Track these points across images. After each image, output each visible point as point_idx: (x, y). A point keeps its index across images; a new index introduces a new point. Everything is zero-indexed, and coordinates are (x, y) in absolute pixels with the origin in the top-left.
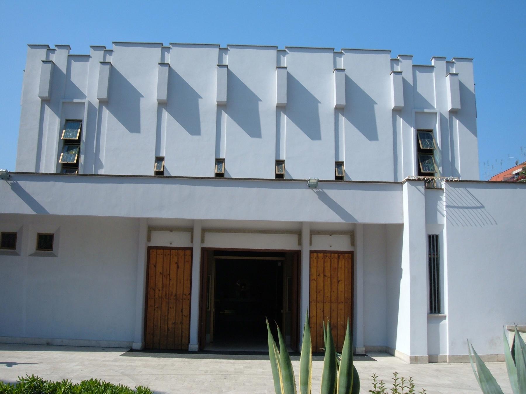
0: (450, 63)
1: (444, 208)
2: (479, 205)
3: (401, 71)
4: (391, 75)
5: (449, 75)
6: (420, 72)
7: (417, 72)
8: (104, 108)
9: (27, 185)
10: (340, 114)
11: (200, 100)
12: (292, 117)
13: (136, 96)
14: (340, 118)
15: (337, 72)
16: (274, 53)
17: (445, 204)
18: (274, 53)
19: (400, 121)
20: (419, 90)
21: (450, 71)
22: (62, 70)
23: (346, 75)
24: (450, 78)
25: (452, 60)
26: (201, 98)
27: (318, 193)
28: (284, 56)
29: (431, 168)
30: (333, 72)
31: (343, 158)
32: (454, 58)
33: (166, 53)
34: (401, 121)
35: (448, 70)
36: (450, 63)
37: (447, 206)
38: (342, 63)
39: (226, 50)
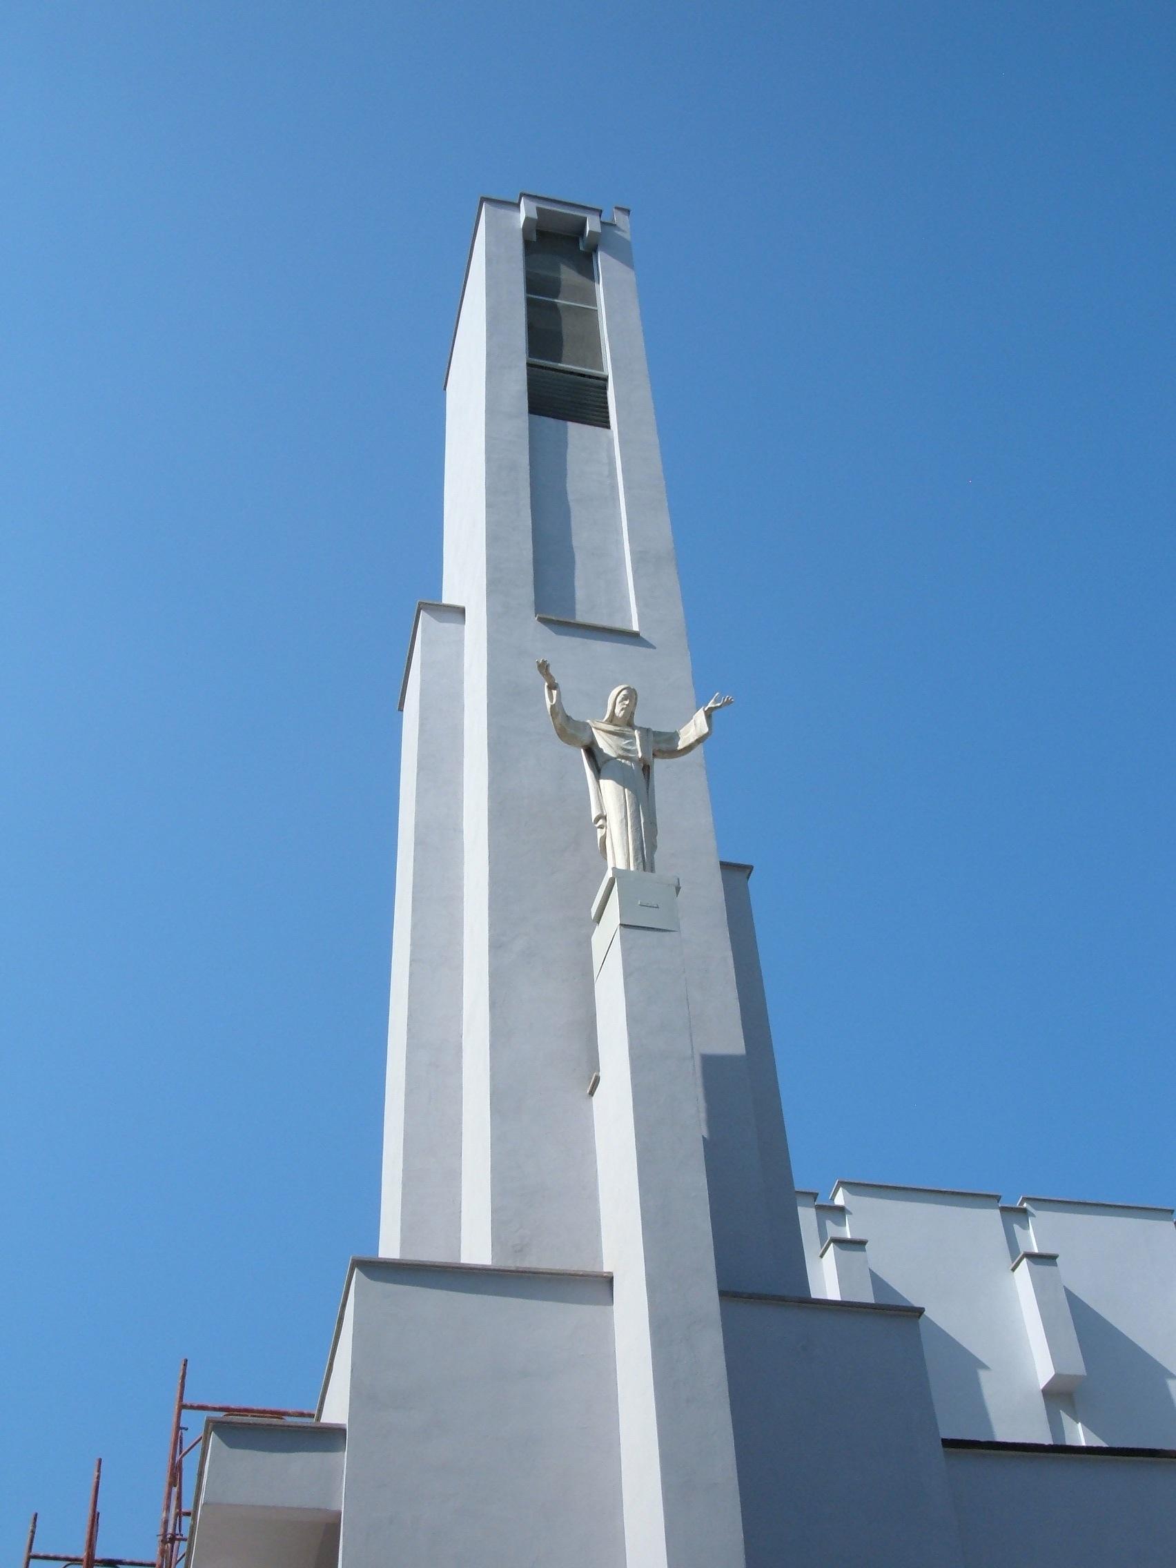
25: (1021, 1203)
32: (1026, 1199)
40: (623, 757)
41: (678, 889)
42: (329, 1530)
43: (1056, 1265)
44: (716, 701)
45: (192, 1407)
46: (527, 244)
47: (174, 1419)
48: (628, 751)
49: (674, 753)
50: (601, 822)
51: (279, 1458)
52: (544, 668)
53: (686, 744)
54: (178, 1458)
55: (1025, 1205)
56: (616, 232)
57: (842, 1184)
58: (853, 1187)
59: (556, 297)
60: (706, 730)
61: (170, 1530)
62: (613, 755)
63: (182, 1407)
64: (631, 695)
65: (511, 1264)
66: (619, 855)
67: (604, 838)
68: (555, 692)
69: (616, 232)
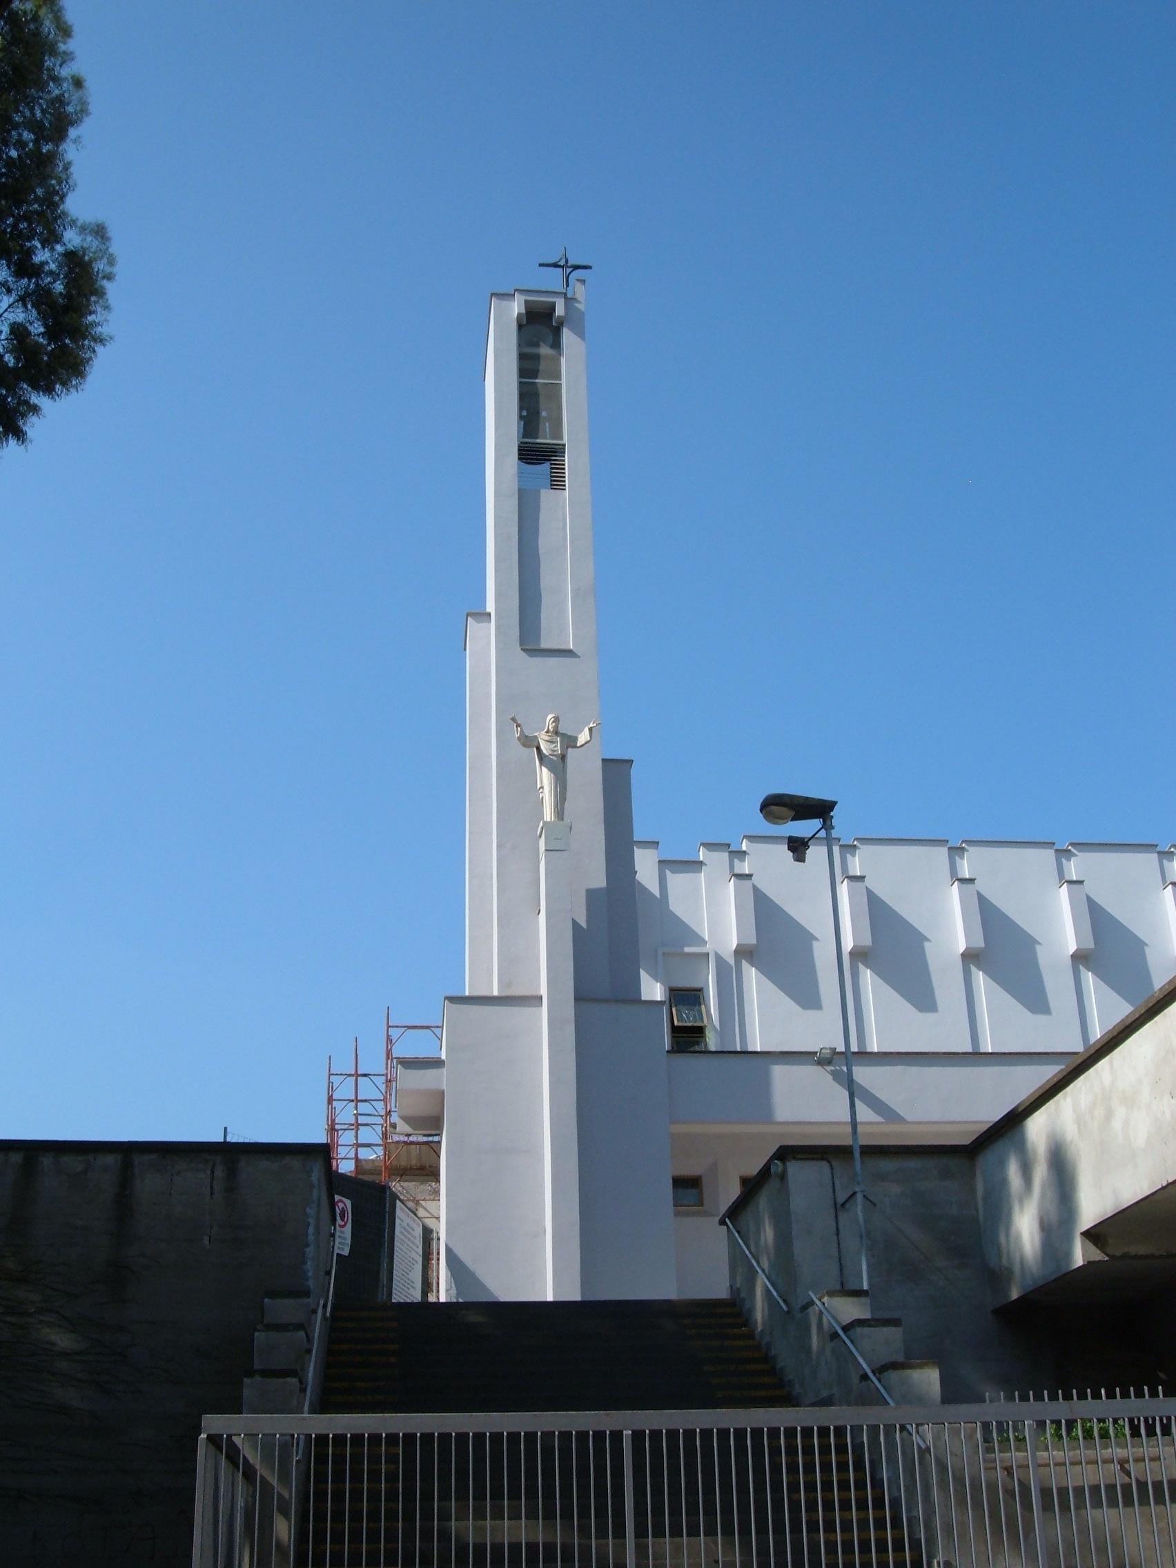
3: (863, 874)
4: (954, 886)
5: (956, 882)
6: (673, 872)
7: (668, 872)
8: (745, 964)
10: (743, 961)
11: (1146, 948)
12: (994, 974)
13: (806, 939)
14: (1082, 977)
15: (736, 880)
16: (1049, 854)
18: (1049, 854)
19: (1088, 976)
21: (957, 875)
22: (652, 890)
23: (754, 887)
24: (1068, 888)
25: (854, 842)
26: (928, 940)
28: (1069, 860)
30: (730, 881)
33: (957, 858)
38: (1073, 869)
39: (853, 848)
40: (551, 755)
41: (571, 829)
42: (443, 1093)
43: (864, 881)
44: (593, 723)
45: (392, 1027)
46: (520, 326)
47: (386, 1032)
48: (554, 751)
49: (575, 747)
50: (541, 790)
51: (422, 1072)
52: (513, 719)
53: (581, 744)
54: (389, 1047)
55: (855, 843)
56: (576, 305)
57: (745, 837)
58: (752, 838)
59: (536, 378)
60: (589, 739)
61: (389, 1077)
62: (548, 754)
63: (389, 1027)
64: (556, 720)
65: (503, 994)
66: (548, 814)
67: (543, 798)
68: (519, 729)
69: (576, 305)
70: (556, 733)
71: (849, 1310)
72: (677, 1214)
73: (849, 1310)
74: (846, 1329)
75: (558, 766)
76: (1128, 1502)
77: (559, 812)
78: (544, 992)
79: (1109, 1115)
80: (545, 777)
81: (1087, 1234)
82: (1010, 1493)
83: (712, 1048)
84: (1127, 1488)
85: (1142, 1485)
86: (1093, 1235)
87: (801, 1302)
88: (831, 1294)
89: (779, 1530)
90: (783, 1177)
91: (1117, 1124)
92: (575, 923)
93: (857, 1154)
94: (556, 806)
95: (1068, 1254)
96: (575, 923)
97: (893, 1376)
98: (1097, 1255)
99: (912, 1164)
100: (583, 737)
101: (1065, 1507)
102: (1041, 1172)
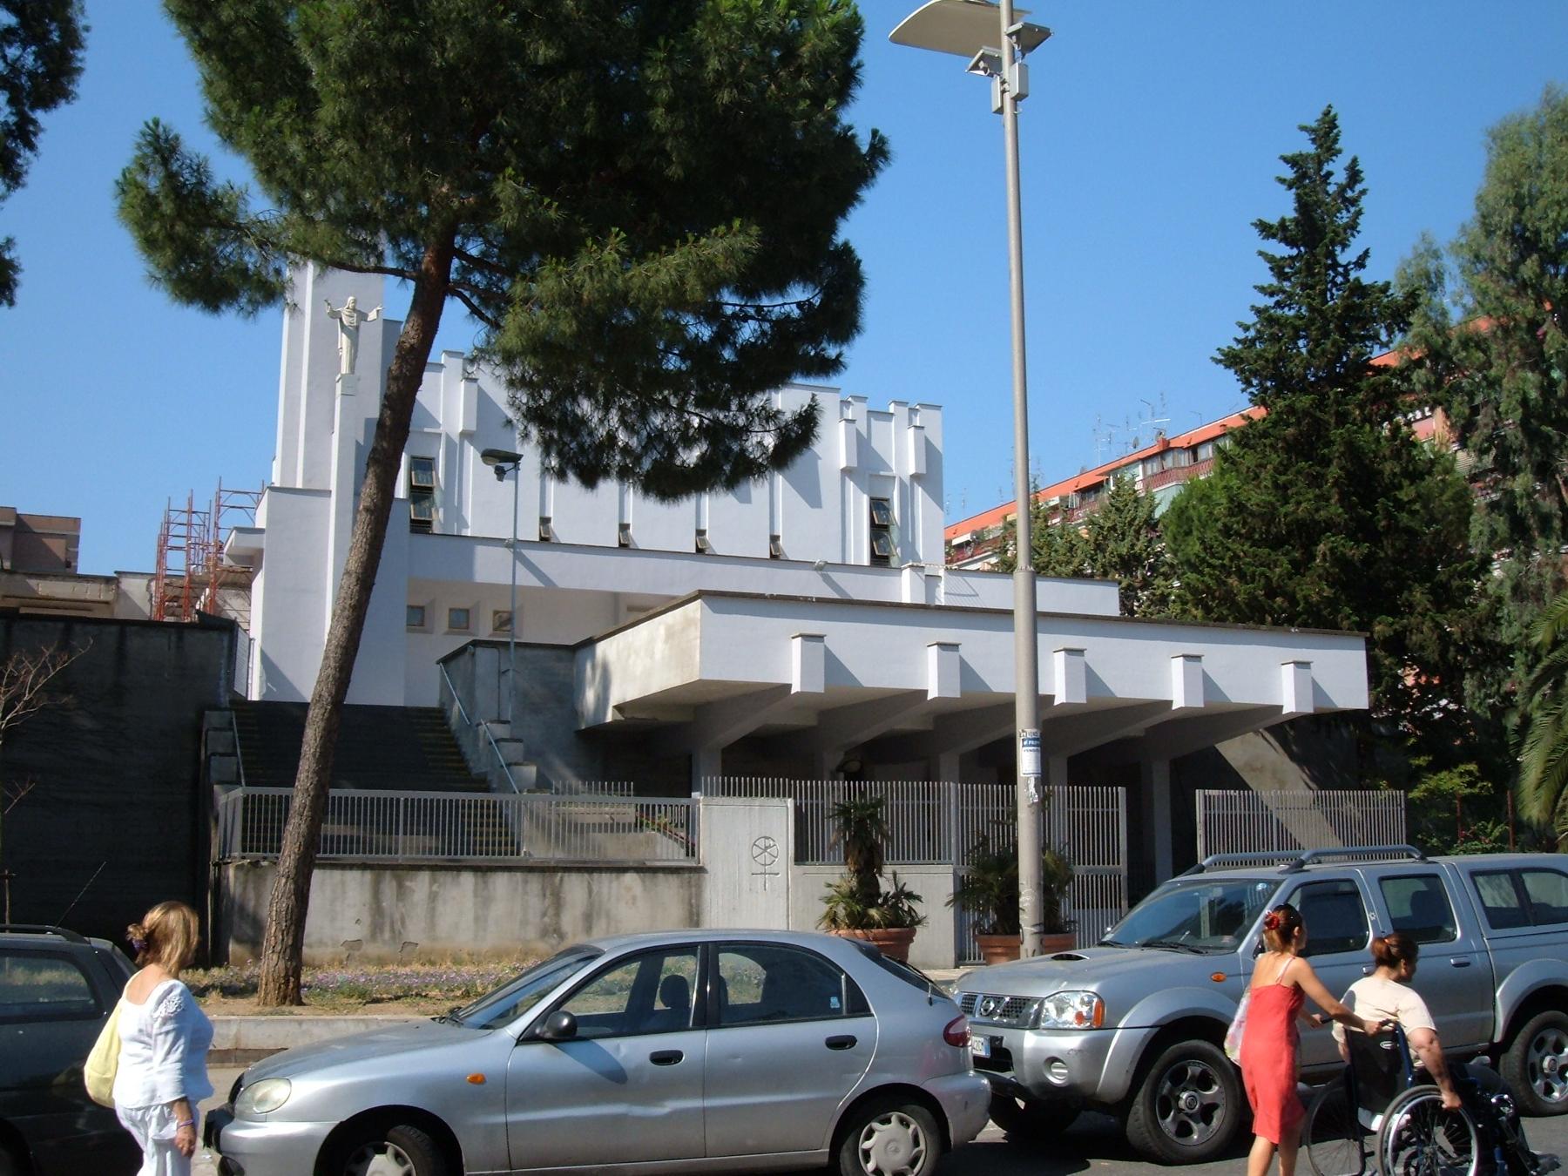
0: (913, 411)
1: (943, 595)
2: (970, 592)
6: (876, 420)
9: (836, 576)
17: (943, 591)
20: (874, 444)
27: (822, 575)
29: (888, 550)
31: (550, 513)
34: (851, 485)
35: (910, 420)
36: (913, 411)
37: (945, 593)
49: (366, 320)
64: (355, 301)
66: (345, 369)
70: (354, 310)
71: (501, 731)
72: (408, 631)
73: (501, 731)
74: (497, 741)
75: (353, 334)
76: (612, 831)
77: (352, 367)
78: (333, 487)
79: (629, 656)
80: (344, 341)
81: (615, 707)
82: (558, 824)
83: (436, 532)
84: (612, 825)
85: (618, 824)
86: (619, 708)
87: (477, 722)
88: (492, 722)
89: (456, 835)
90: (473, 655)
91: (631, 662)
92: (357, 442)
93: (512, 645)
94: (350, 363)
95: (605, 714)
96: (357, 442)
97: (515, 768)
98: (619, 717)
99: (541, 652)
100: (372, 315)
101: (582, 832)
102: (599, 672)
